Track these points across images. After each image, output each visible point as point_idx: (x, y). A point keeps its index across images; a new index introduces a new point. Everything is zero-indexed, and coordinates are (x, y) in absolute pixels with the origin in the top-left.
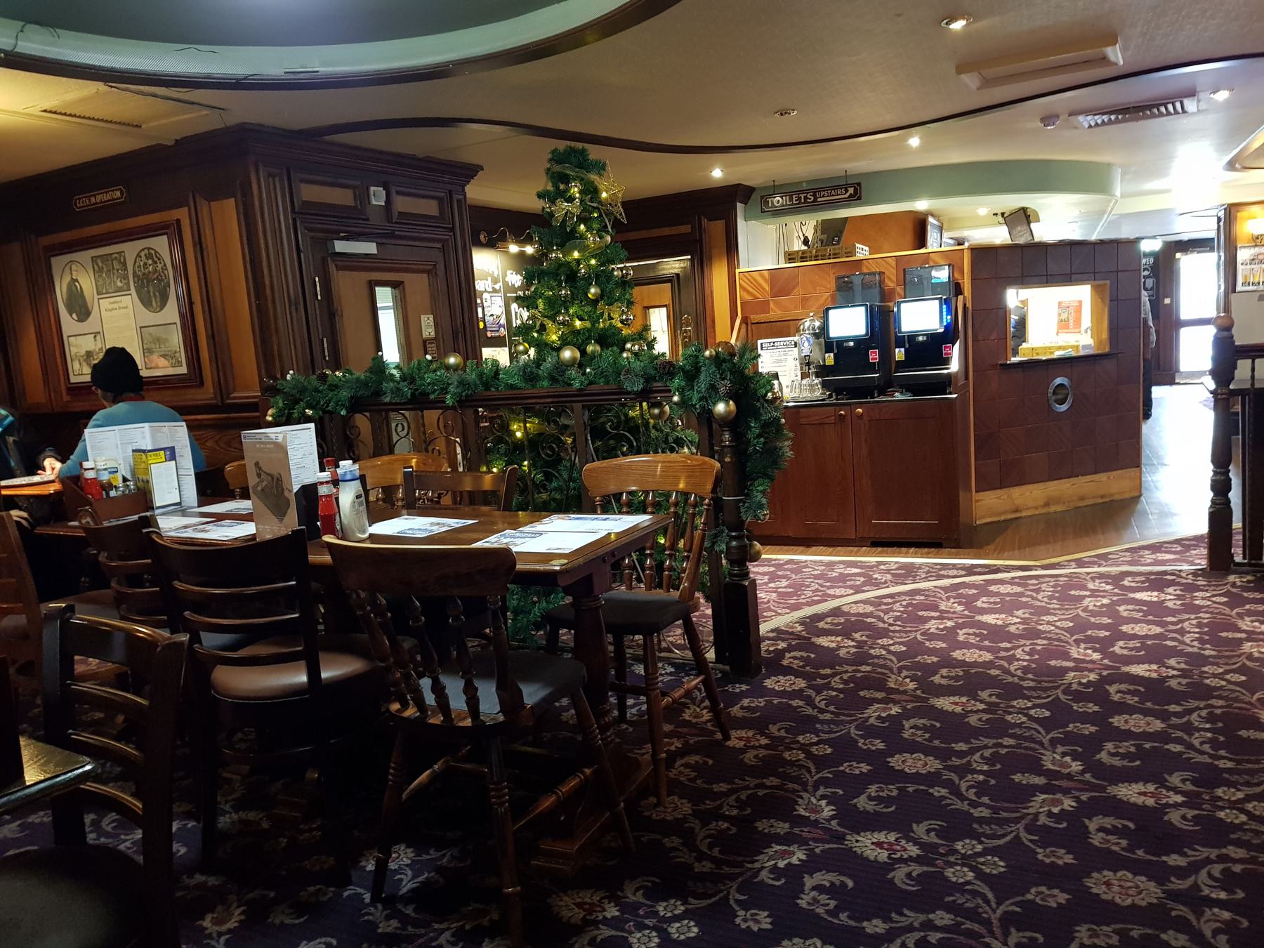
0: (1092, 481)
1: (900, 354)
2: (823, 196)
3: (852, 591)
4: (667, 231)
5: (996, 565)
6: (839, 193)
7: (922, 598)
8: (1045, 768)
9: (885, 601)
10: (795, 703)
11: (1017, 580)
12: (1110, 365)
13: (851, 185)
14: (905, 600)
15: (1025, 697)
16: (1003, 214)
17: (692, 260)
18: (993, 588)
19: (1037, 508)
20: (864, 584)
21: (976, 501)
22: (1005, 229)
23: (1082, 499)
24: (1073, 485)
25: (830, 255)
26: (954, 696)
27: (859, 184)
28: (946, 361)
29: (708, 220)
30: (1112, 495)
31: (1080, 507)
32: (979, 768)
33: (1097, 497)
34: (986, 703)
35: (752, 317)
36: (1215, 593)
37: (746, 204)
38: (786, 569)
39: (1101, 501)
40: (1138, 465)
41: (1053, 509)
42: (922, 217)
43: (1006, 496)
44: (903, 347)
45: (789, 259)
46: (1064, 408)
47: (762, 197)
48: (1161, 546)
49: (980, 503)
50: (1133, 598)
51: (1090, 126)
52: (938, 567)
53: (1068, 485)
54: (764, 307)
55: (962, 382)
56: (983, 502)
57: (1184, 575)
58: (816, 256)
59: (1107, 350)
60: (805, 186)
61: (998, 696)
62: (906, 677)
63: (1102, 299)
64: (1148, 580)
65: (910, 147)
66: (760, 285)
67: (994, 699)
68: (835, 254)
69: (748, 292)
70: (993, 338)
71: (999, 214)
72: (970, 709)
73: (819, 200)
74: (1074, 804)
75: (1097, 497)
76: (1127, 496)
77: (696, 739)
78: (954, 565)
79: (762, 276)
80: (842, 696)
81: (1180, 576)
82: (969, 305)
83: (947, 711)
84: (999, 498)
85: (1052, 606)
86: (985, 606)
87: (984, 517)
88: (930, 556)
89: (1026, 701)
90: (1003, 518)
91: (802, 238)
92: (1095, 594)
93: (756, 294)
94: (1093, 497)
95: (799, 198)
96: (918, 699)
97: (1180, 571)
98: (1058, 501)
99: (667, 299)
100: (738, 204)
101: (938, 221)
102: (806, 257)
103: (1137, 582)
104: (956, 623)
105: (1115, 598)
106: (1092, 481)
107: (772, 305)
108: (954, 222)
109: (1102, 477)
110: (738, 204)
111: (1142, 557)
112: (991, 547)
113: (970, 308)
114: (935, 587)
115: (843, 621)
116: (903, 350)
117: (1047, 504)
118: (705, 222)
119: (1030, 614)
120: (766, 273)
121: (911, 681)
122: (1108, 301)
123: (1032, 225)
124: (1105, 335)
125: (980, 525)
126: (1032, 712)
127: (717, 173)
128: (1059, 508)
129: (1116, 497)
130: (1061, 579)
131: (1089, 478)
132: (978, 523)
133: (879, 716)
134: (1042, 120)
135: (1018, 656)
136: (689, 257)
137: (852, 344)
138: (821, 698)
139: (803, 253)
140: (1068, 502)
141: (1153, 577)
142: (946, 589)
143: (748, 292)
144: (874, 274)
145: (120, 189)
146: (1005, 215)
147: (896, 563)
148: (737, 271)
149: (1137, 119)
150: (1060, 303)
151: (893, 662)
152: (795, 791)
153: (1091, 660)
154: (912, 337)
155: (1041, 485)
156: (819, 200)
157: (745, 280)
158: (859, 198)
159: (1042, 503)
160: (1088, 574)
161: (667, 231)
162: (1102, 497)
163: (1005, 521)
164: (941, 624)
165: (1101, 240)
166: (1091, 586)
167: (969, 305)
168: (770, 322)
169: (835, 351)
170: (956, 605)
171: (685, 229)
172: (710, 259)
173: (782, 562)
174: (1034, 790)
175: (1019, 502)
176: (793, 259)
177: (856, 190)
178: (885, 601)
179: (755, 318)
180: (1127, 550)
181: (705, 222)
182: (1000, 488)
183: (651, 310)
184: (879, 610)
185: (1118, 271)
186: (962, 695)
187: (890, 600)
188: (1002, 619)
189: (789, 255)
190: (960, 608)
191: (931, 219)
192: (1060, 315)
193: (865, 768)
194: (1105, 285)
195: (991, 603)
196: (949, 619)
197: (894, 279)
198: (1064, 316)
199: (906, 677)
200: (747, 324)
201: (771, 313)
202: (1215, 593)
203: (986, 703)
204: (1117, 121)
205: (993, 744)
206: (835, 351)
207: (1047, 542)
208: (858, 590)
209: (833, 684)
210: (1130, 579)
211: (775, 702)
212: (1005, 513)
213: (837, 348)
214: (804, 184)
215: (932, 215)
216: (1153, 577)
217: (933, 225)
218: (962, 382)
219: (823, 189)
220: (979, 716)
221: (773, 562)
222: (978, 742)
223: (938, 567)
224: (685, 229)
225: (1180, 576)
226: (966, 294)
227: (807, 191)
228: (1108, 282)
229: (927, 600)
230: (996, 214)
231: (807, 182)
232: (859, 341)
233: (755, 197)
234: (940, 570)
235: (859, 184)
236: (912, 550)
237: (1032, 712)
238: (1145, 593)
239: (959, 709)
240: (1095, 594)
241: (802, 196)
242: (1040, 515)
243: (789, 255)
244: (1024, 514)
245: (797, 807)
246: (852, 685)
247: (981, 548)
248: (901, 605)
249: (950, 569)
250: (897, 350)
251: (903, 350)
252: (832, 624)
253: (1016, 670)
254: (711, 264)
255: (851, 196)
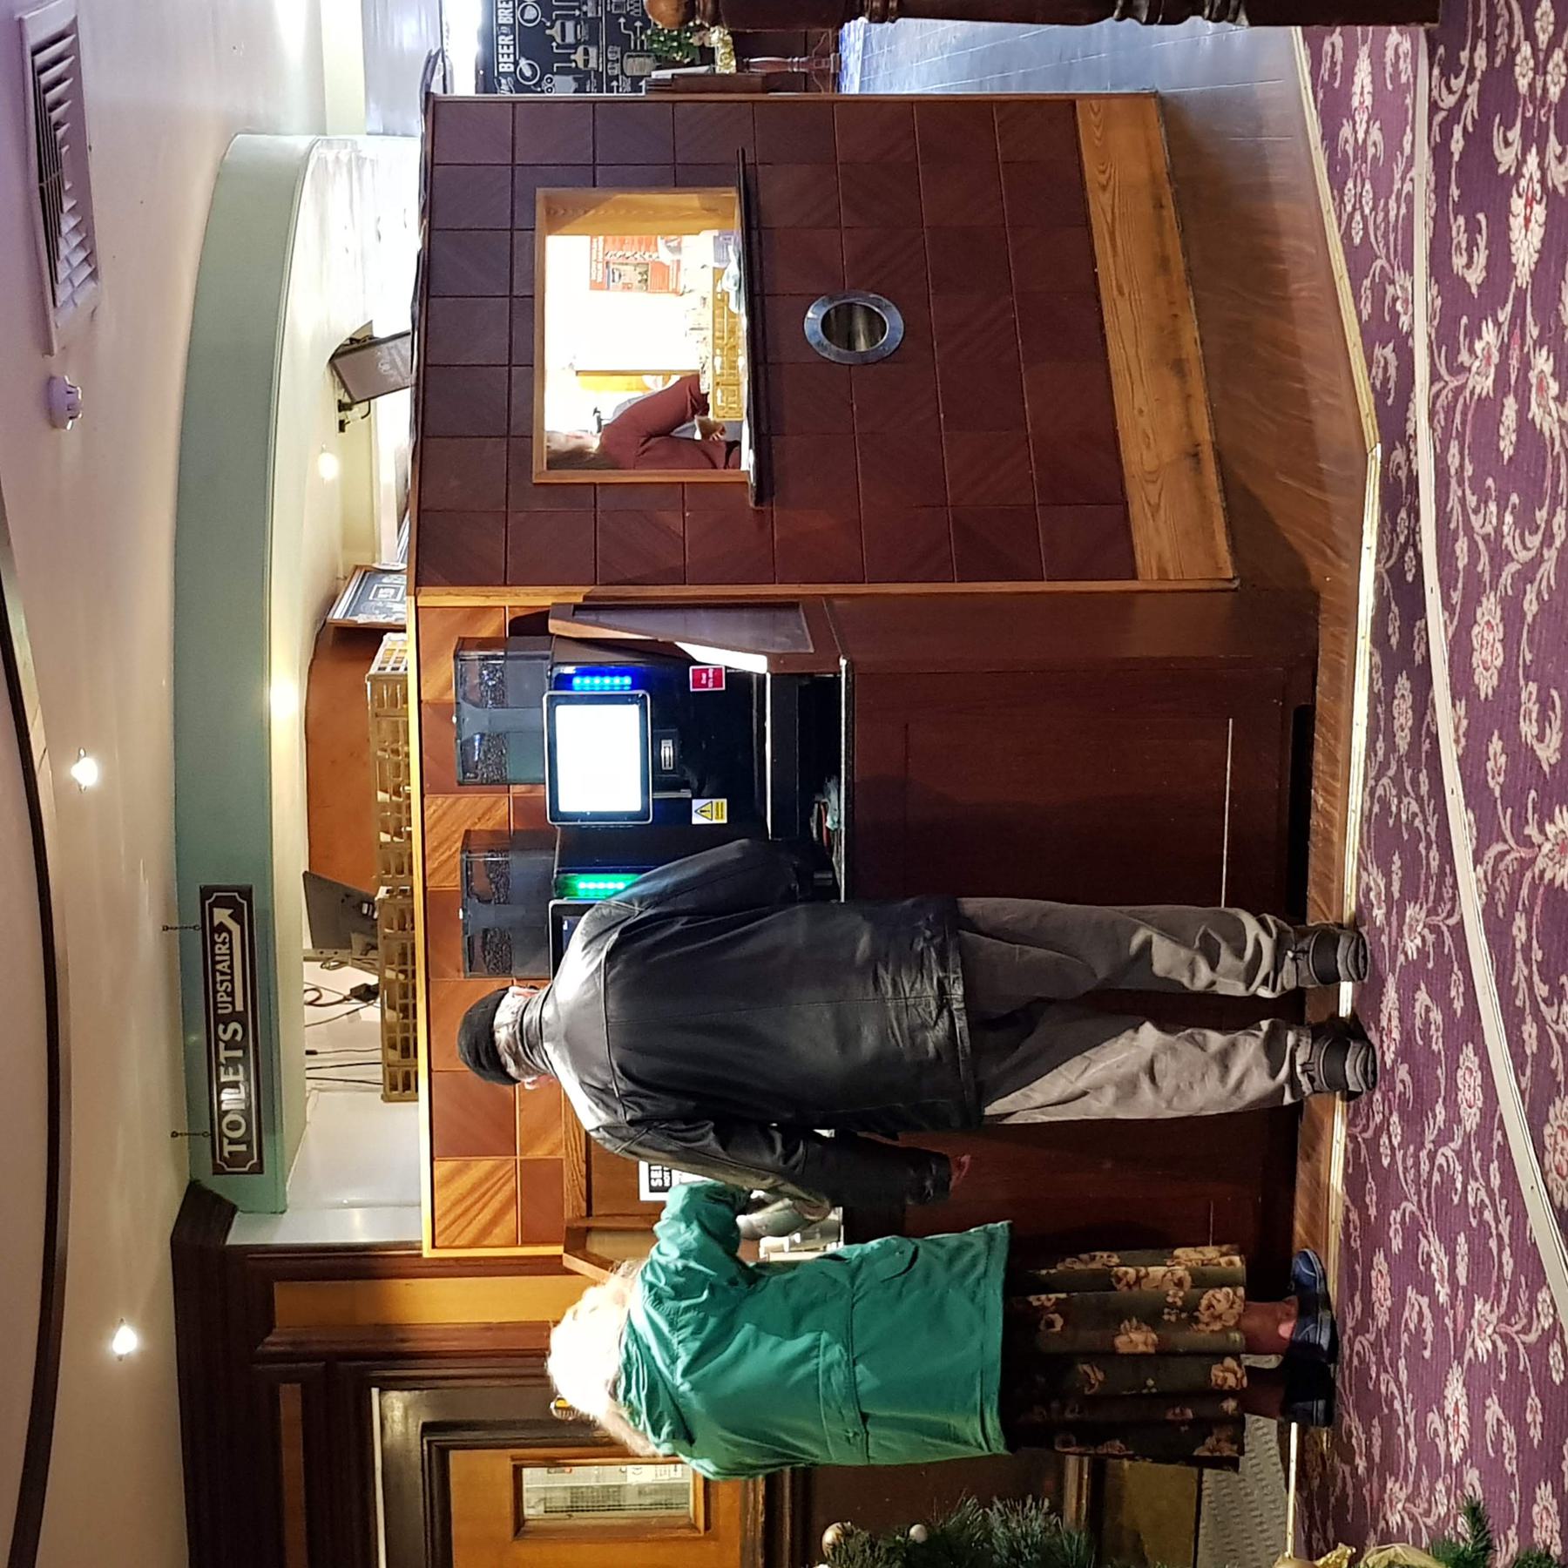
0: (1112, 234)
1: (708, 812)
2: (231, 994)
3: (1469, 1050)
4: (292, 1458)
5: (1378, 577)
6: (225, 949)
7: (1520, 921)
8: (1491, 394)
9: (1531, 1046)
10: (1531, 607)
11: (1456, 597)
12: (776, 187)
13: (206, 915)
14: (1463, 500)
15: (1510, 63)
16: (342, 407)
17: (386, 1386)
18: (1486, 683)
19: (1187, 398)
20: (1441, 997)
21: (1163, 575)
22: (382, 403)
23: (1164, 263)
24: (1121, 293)
25: (404, 972)
26: (1509, 228)
27: (206, 892)
28: (739, 681)
29: (269, 1333)
30: (1154, 178)
31: (1189, 270)
32: (1494, 521)
33: (1160, 220)
34: (1525, 150)
35: (568, 1214)
36: (1519, 30)
37: (233, 1210)
38: (1383, 1215)
39: (1170, 212)
40: (1069, 105)
41: (1191, 348)
42: (329, 636)
43: (1150, 487)
44: (689, 801)
45: (407, 1087)
46: (894, 322)
47: (218, 1171)
48: (1327, 86)
49: (1170, 568)
50: (1532, 274)
51: (94, 275)
52: (1380, 745)
53: (1123, 306)
54: (539, 1178)
55: (799, 624)
56: (1167, 555)
57: (1449, 101)
58: (404, 1009)
59: (733, 194)
60: (197, 1038)
61: (1508, 126)
62: (1542, 831)
63: (596, 204)
64: (1467, 207)
65: (108, 777)
66: (474, 1189)
67: (1514, 134)
68: (405, 996)
69: (494, 1221)
70: (677, 525)
71: (342, 415)
72: (1537, 187)
73: (239, 1007)
74: (1544, 352)
75: (1160, 220)
76: (1159, 133)
77: (1450, 1326)
78: (1374, 698)
79: (450, 1178)
80: (1514, 499)
81: (1455, 114)
82: (576, 595)
83: (1543, 241)
84: (1155, 509)
85: (1392, 204)
86: (1481, 258)
87: (1212, 555)
88: (1340, 755)
89: (1518, 59)
90: (1216, 499)
91: (355, 1004)
92: (1513, 382)
93: (501, 1197)
94: (1160, 234)
95: (231, 1062)
96: (1518, 317)
97: (1434, 107)
98: (1168, 335)
99: (497, 1464)
100: (233, 1239)
101: (347, 579)
102: (406, 1040)
103: (1472, 243)
104: (1539, 343)
105: (1534, 331)
106: (1112, 234)
107: (539, 1153)
108: (357, 533)
109: (1100, 206)
110: (233, 1239)
111: (1361, 149)
112: (1314, 563)
113: (586, 589)
114: (1477, 860)
115: (1533, 687)
116: (696, 804)
117: (1179, 367)
118: (275, 1342)
119: (1374, 156)
120: (443, 1168)
121: (1552, 821)
122: (595, 193)
123: (379, 333)
124: (691, 200)
125: (1236, 567)
126: (1543, 39)
127: (125, 1341)
128: (1190, 333)
129: (1162, 160)
130: (1453, 461)
131: (1101, 245)
132: (1230, 575)
133: (1557, 399)
134: (55, 422)
135: (1489, 529)
136: (375, 1391)
137: (667, 750)
138: (1519, 546)
139: (393, 1047)
140: (1172, 303)
141: (1455, 192)
142: (1486, 834)
143: (494, 1221)
144: (468, 867)
145: (378, 588)
146: (347, 400)
147: (1362, 866)
148: (427, 1252)
149: (81, 151)
150: (595, 286)
151: (1502, 855)
152: (1534, 887)
153: (1500, 350)
154: (656, 777)
155: (1120, 383)
156: (239, 1007)
157: (455, 1229)
158: (247, 893)
159: (1173, 384)
160: (1435, 377)
161: (292, 1458)
162: (1159, 206)
163: (1226, 490)
164: (1542, 389)
165: (423, 211)
166: (1484, 384)
167: (576, 595)
168: (588, 1162)
169: (686, 793)
170: (1479, 346)
171: (290, 1402)
172: (386, 1329)
173: (1354, 1216)
174: (1525, 425)
175: (1167, 449)
176: (407, 1075)
177: (220, 903)
178: (1531, 1046)
179: (572, 1206)
180: (1338, 184)
181: (275, 1342)
182: (1124, 503)
183: (528, 1512)
184: (1496, 577)
185: (510, 364)
186: (1507, 211)
187: (1530, 1029)
188: (1529, 204)
189: (394, 1088)
190: (1489, 334)
191: (338, 614)
192: (627, 287)
193: (1496, 745)
194: (548, 199)
195: (1472, 243)
196: (1526, 365)
197: (488, 799)
198: (631, 274)
199: (1542, 831)
200: (589, 1230)
201: (561, 1154)
202: (1519, 30)
203: (1525, 150)
204: (84, 210)
205: (1459, 486)
206: (686, 793)
207: (1302, 399)
208: (1467, 1028)
209: (1489, 529)
210: (1459, 261)
211: (1529, 657)
212: (1200, 491)
213: (677, 789)
214: (193, 1038)
215: (331, 601)
216: (1455, 192)
217: (354, 608)
218: (799, 624)
219: (209, 991)
220: (1553, 163)
221: (1356, 1244)
222: (1455, 517)
223: (1380, 745)
224: (290, 1402)
225: (1455, 114)
226: (547, 601)
227: (212, 1041)
228: (540, 192)
229: (1461, 436)
230: (342, 426)
231: (187, 1028)
232: (659, 725)
233: (215, 1184)
234: (1391, 747)
235: (206, 892)
236: (1318, 798)
237: (1543, 39)
238: (1516, 233)
239: (1539, 212)
240: (1513, 382)
241: (224, 1054)
242: (1208, 387)
243: (394, 1088)
244: (1205, 436)
245: (1484, 394)
246: (1490, 482)
247: (1317, 596)
248: (1476, 511)
249: (1390, 718)
250: (697, 820)
251: (696, 804)
252: (1543, 720)
253: (1450, 91)
254: (401, 1327)
255: (238, 917)
